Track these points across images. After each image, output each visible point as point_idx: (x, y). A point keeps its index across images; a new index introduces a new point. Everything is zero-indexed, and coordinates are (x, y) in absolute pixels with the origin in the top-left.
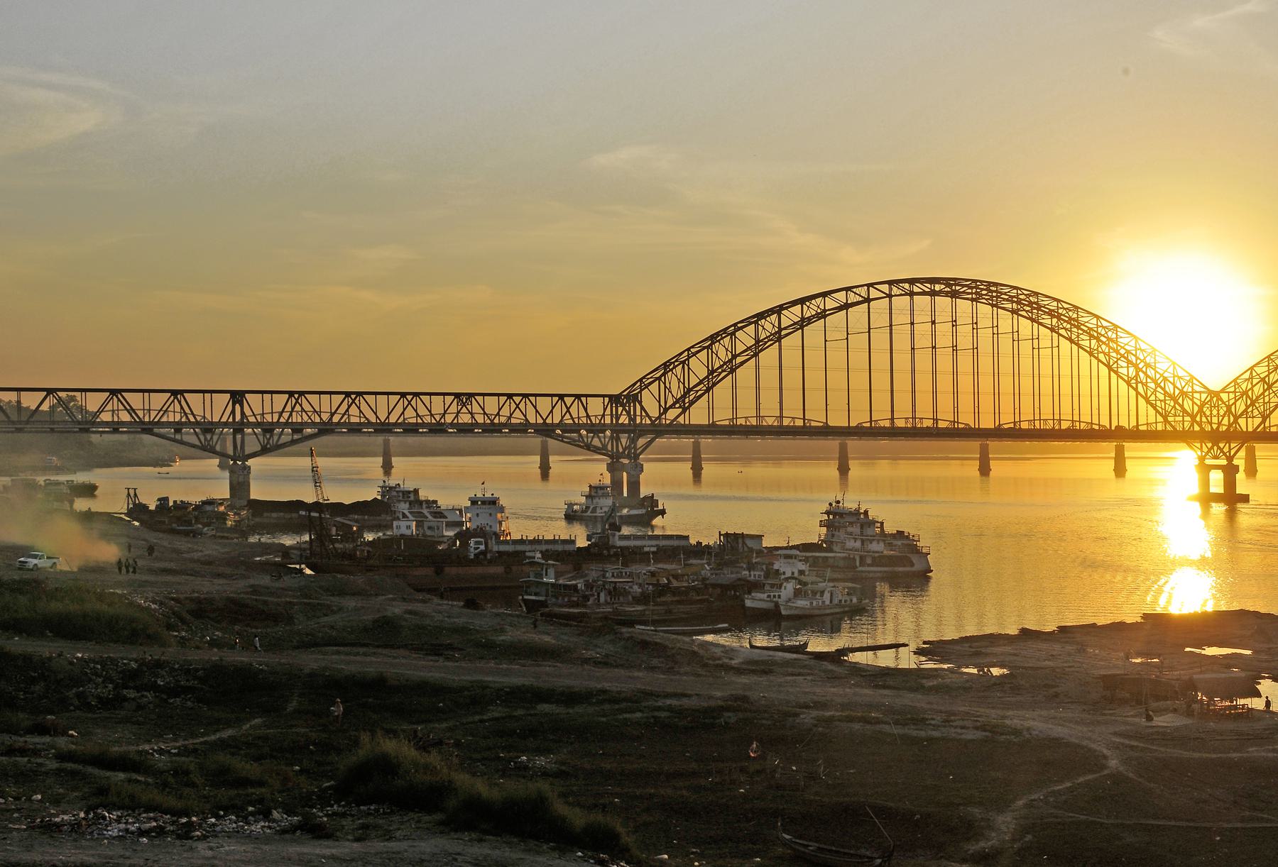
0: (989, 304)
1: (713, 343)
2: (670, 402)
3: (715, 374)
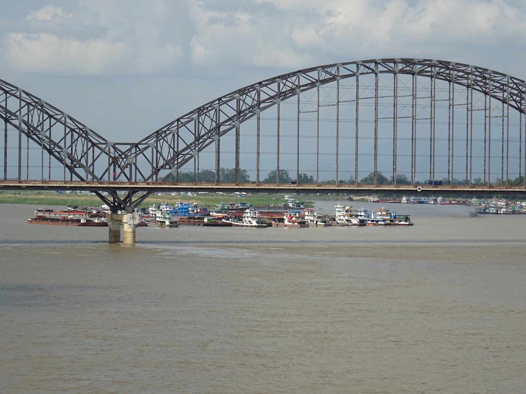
0: (447, 80)
1: (200, 115)
2: (161, 163)
3: (201, 141)
